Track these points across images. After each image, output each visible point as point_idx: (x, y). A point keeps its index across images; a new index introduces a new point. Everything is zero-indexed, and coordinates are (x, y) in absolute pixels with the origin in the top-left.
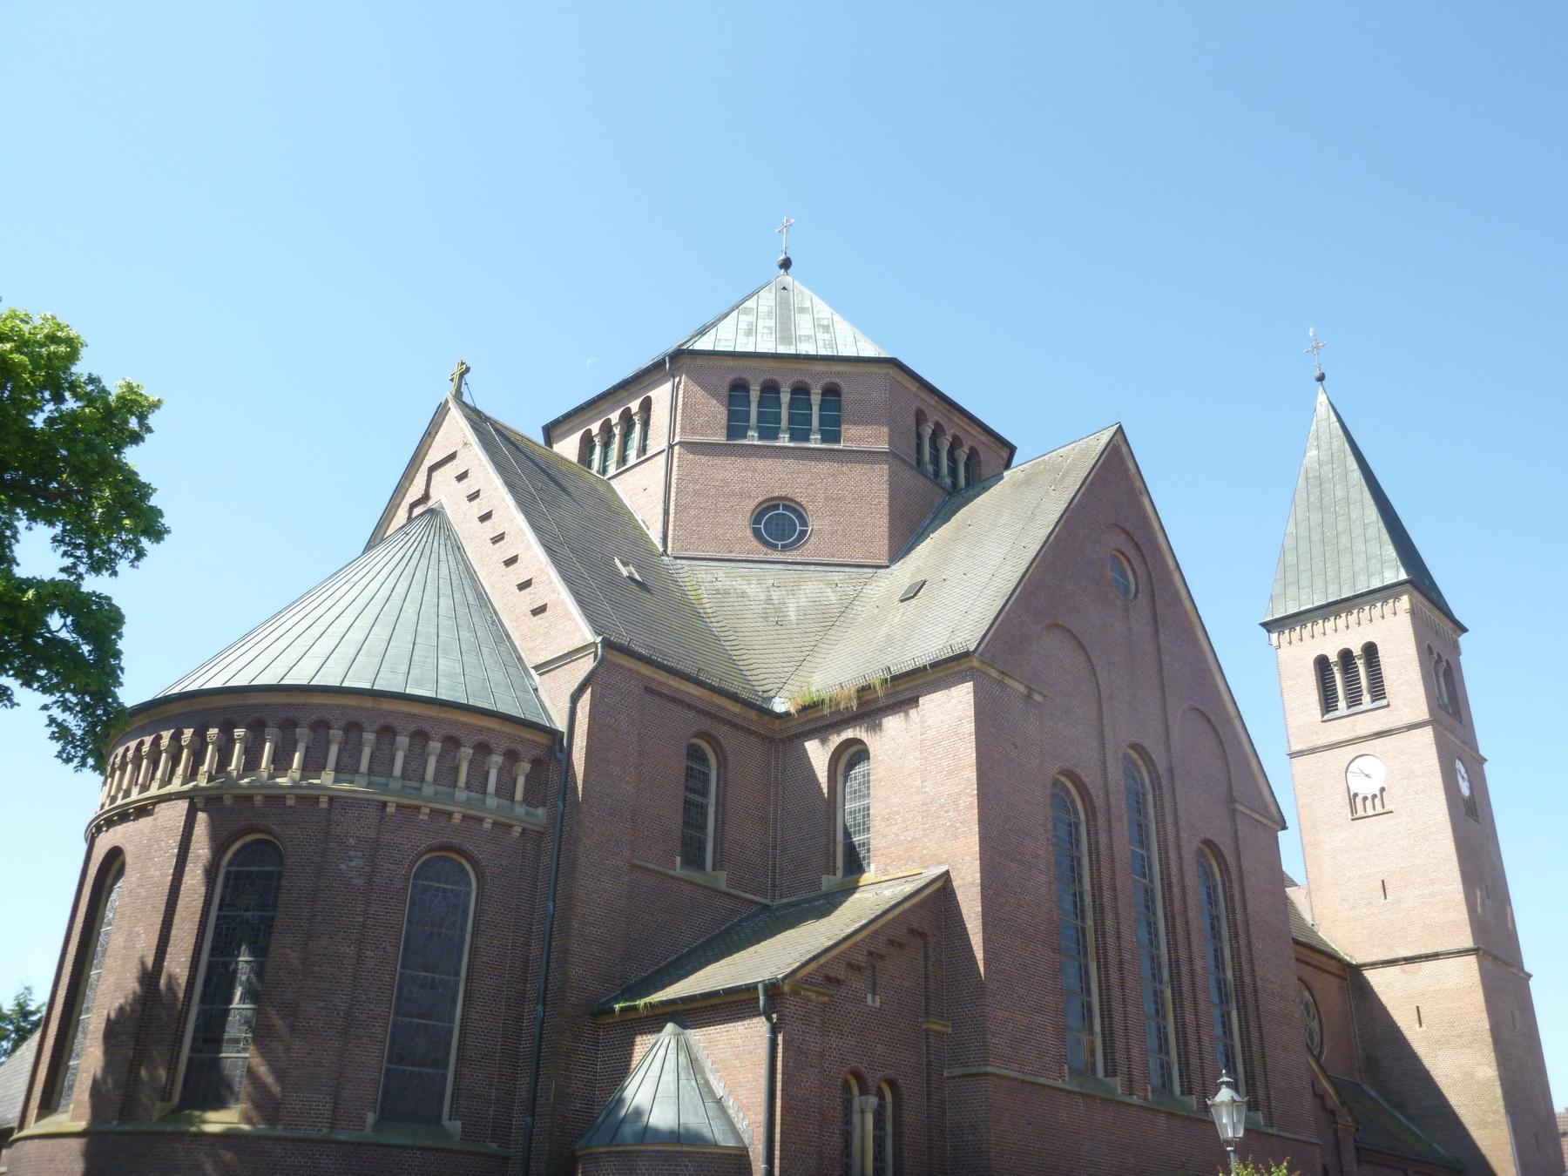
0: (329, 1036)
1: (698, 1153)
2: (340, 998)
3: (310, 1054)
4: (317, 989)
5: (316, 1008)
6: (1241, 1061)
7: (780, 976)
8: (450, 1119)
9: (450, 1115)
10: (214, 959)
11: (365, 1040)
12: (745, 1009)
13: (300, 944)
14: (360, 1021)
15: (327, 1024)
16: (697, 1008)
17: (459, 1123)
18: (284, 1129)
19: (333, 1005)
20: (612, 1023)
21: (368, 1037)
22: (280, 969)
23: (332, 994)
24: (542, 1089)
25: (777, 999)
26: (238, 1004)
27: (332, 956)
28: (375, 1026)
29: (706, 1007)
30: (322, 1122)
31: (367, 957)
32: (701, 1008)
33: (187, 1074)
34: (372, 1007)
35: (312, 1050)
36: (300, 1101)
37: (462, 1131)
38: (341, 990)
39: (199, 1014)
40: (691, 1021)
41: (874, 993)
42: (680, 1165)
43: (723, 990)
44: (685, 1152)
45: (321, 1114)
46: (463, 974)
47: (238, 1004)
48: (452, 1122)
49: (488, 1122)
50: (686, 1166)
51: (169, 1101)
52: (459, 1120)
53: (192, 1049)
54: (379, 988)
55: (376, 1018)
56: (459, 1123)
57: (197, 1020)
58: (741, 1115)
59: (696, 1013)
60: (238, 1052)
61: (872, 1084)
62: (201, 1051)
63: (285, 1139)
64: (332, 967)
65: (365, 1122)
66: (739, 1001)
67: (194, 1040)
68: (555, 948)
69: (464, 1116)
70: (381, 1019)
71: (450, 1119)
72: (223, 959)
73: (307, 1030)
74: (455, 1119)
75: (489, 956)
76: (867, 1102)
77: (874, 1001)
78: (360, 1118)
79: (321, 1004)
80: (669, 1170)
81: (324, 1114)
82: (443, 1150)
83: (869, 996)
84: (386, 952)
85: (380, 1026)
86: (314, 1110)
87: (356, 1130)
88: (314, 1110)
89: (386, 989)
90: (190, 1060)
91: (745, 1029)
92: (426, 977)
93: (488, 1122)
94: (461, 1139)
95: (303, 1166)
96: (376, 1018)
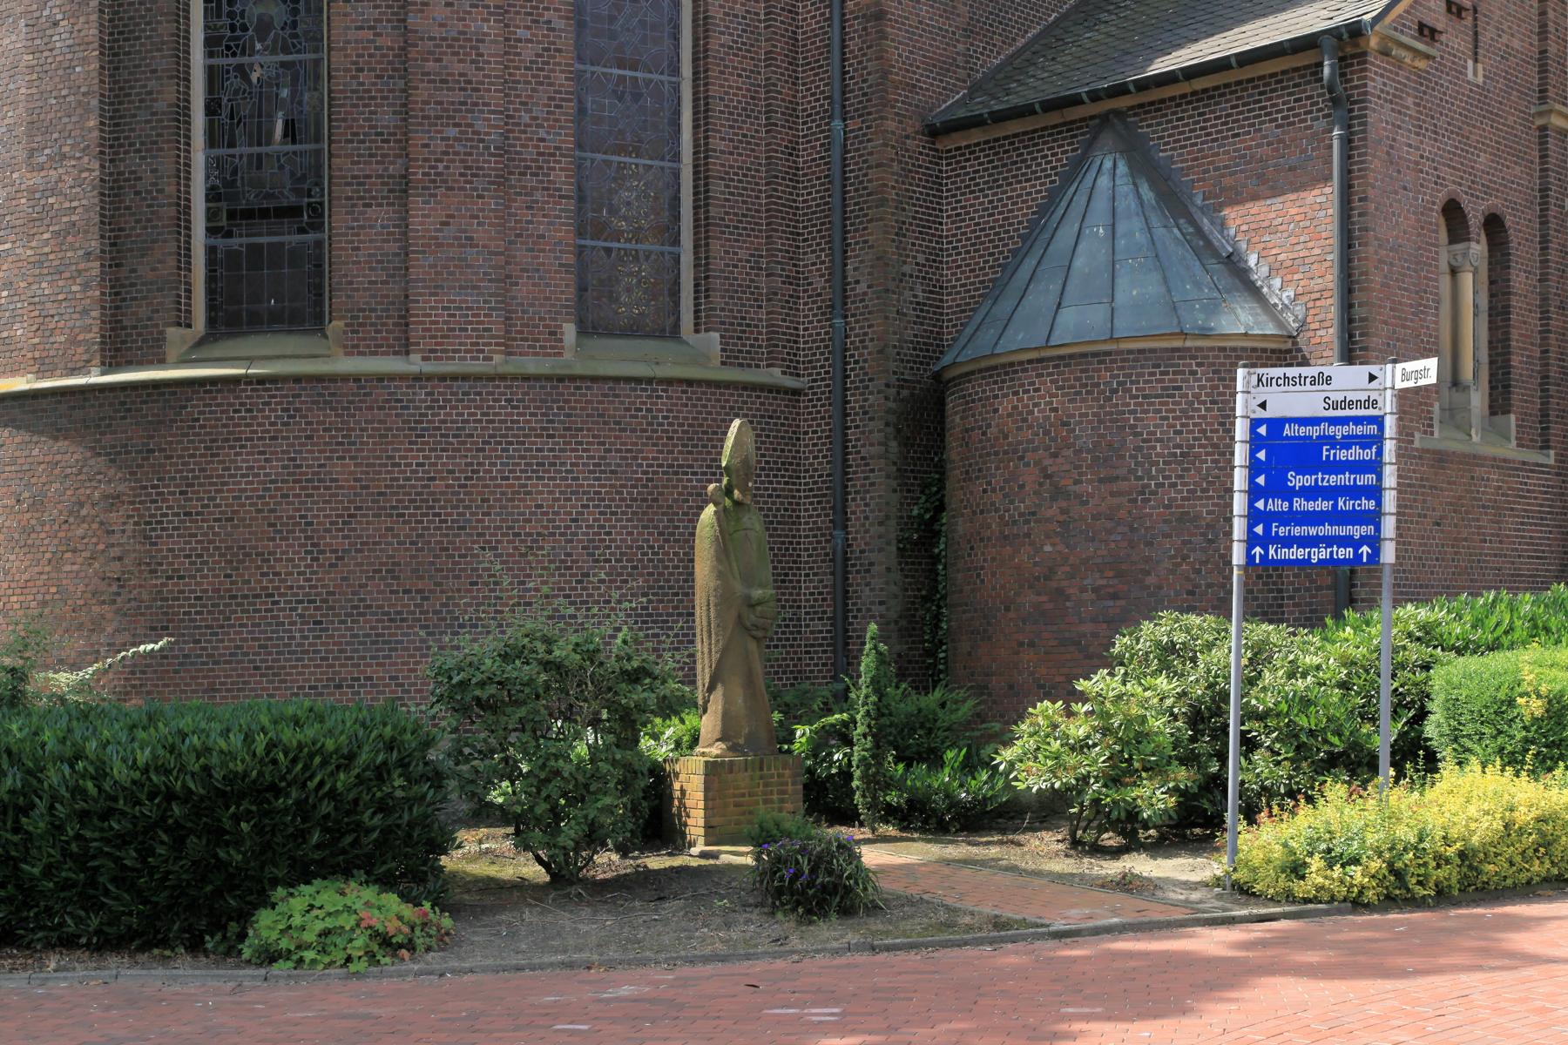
0: (476, 189)
1: (1212, 349)
2: (485, 119)
3: (447, 224)
4: (437, 103)
5: (442, 139)
6: (683, 294)
7: (1367, 17)
8: (697, 331)
9: (696, 324)
10: (216, 61)
11: (538, 196)
12: (1274, 90)
13: (388, 21)
14: (525, 160)
15: (470, 168)
16: (1162, 101)
17: (716, 336)
18: (424, 359)
19: (474, 133)
20: (968, 147)
21: (544, 189)
22: (361, 70)
23: (468, 111)
24: (855, 269)
25: (1352, 65)
26: (282, 143)
27: (457, 40)
28: (554, 169)
29: (1184, 96)
30: (490, 344)
31: (519, 40)
32: (1172, 99)
33: (211, 279)
34: (542, 133)
35: (448, 216)
36: (444, 308)
37: (723, 350)
38: (485, 104)
39: (208, 167)
40: (1149, 126)
41: (1476, 61)
42: (1183, 373)
43: (1181, 69)
44: (1189, 349)
45: (485, 330)
46: (687, 70)
47: (282, 143)
48: (702, 335)
49: (760, 333)
50: (1193, 373)
51: (189, 326)
52: (716, 330)
53: (211, 231)
54: (550, 99)
55: (553, 155)
56: (716, 336)
57: (207, 177)
58: (1277, 282)
59: (1160, 110)
60: (302, 231)
61: (1475, 220)
62: (229, 234)
63: (429, 377)
64: (460, 61)
65: (561, 341)
66: (1261, 78)
67: (211, 215)
68: (852, 12)
69: (723, 323)
70: (562, 155)
71: (697, 331)
72: (238, 60)
73: (434, 181)
74: (707, 330)
75: (731, 34)
76: (1465, 255)
77: (1475, 73)
78: (551, 333)
79: (452, 132)
80: (1162, 381)
81: (490, 330)
82: (699, 382)
83: (1470, 63)
84: (553, 30)
85: (561, 169)
86: (471, 323)
87: (549, 355)
88: (471, 323)
89: (563, 100)
90: (211, 251)
91: (1277, 127)
92: (622, 79)
93: (760, 333)
94: (723, 363)
95: (467, 421)
96: (553, 155)
